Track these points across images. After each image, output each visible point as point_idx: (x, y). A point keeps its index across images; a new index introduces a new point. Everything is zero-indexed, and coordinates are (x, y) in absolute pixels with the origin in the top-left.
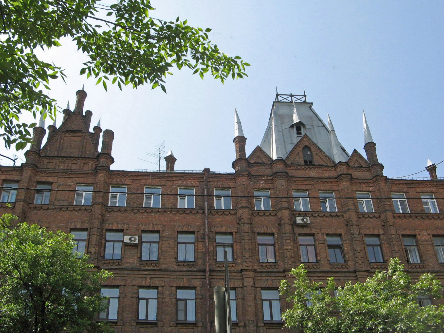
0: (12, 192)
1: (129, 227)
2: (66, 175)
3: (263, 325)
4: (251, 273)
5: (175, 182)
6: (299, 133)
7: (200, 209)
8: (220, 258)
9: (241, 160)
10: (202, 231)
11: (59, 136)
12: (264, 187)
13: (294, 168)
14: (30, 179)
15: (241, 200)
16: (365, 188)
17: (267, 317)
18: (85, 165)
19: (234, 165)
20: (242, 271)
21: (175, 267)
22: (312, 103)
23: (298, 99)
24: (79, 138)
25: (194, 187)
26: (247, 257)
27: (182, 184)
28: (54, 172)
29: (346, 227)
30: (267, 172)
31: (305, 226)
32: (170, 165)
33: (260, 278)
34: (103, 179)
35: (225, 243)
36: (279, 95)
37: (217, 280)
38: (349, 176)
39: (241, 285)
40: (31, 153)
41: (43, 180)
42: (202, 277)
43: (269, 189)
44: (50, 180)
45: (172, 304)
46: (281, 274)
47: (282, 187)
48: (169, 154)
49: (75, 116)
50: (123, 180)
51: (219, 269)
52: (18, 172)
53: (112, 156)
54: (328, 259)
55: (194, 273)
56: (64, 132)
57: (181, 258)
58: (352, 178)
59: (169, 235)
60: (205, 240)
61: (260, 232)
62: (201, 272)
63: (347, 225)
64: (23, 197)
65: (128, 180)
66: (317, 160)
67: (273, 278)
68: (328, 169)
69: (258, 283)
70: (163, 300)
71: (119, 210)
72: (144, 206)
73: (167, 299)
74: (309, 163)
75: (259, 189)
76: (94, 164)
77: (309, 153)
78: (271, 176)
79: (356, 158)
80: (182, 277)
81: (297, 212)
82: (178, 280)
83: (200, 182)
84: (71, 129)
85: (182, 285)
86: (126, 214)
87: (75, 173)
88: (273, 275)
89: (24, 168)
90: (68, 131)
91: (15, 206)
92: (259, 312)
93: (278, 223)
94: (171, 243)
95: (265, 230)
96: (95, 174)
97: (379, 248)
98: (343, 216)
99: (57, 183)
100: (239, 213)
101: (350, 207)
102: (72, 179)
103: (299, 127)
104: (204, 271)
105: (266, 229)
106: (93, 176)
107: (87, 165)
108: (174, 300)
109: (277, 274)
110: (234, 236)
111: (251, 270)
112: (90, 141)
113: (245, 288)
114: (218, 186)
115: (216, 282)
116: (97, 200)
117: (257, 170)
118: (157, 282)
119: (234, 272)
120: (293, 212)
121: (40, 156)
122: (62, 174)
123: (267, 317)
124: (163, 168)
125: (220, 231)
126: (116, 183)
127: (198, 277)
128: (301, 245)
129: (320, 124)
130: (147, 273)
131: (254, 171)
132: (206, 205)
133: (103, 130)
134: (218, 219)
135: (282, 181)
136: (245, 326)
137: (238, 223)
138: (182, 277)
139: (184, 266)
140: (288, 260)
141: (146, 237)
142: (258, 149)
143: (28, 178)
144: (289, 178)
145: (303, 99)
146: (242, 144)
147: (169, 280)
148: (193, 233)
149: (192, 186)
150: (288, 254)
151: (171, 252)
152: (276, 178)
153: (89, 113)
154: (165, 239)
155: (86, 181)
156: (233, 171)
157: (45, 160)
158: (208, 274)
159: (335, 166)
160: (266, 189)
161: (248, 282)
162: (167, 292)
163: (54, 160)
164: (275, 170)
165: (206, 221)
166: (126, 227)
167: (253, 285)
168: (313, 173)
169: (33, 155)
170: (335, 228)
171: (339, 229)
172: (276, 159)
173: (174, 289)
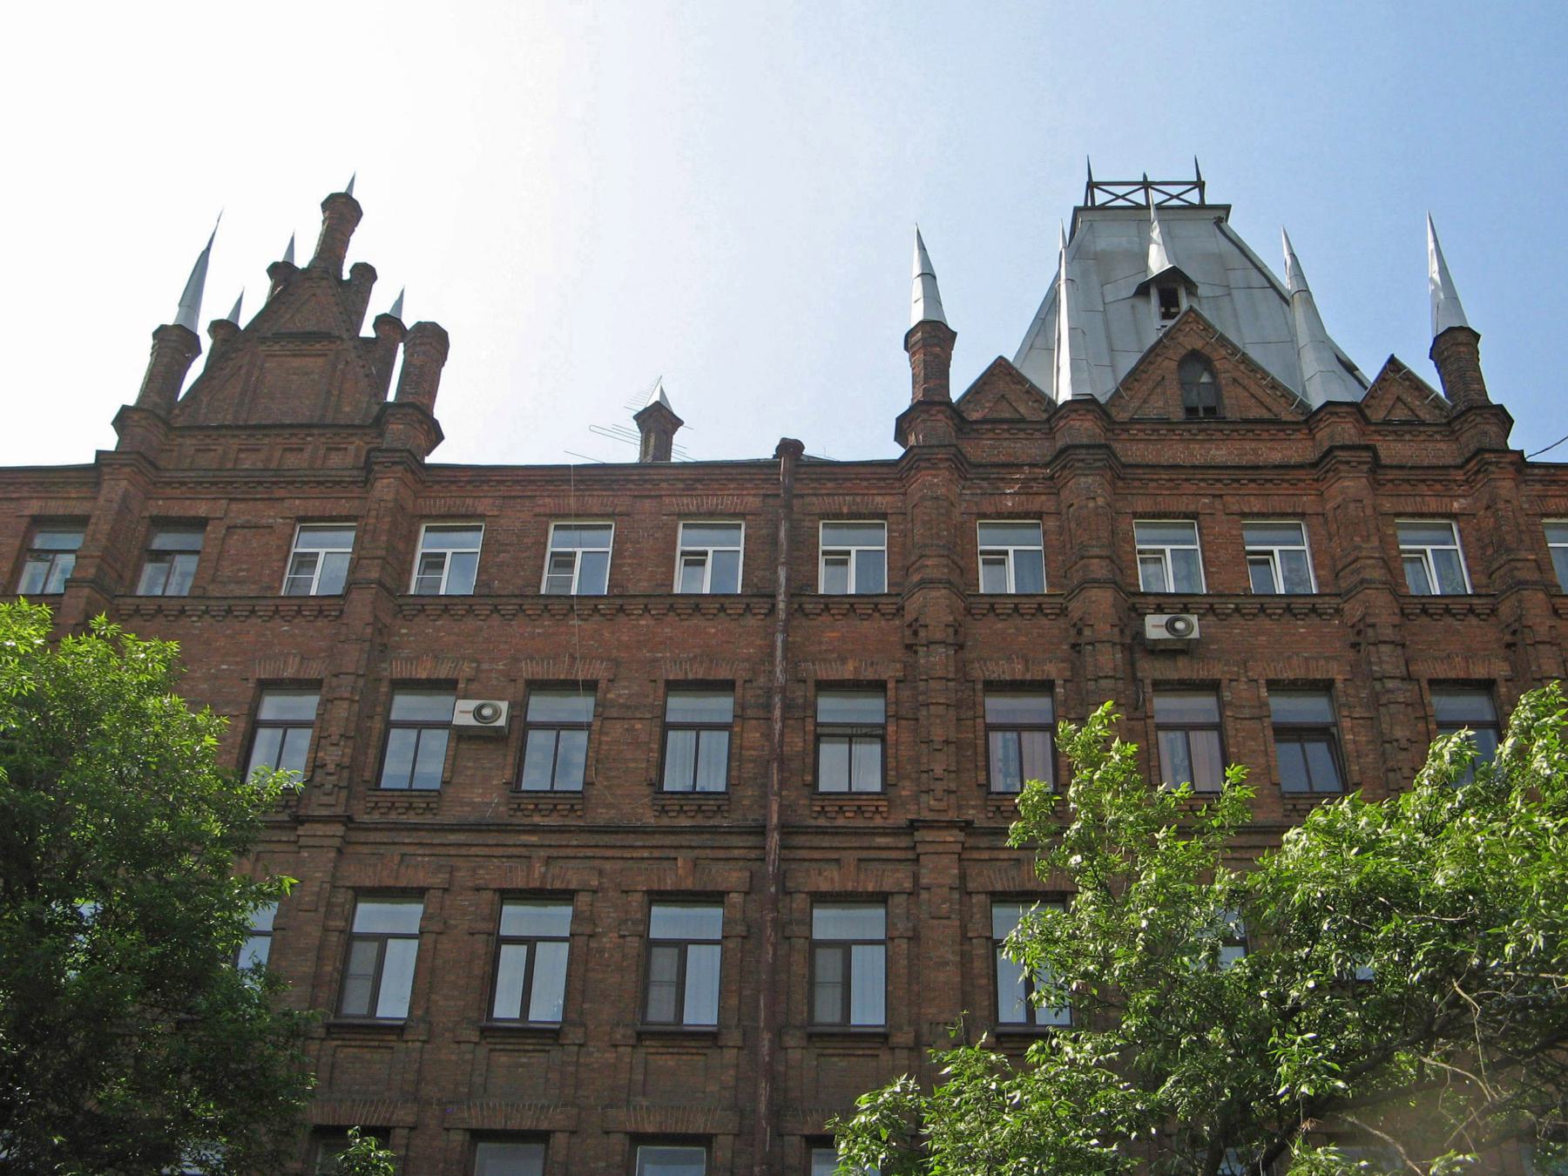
1: (478, 670)
2: (260, 489)
4: (950, 836)
5: (667, 500)
9: (929, 410)
15: (921, 557)
18: (333, 455)
19: (903, 427)
20: (913, 826)
21: (650, 819)
22: (1227, 208)
24: (321, 360)
26: (939, 771)
27: (693, 509)
31: (1183, 652)
32: (652, 441)
33: (986, 855)
34: (390, 497)
37: (814, 865)
38: (1366, 456)
41: (176, 510)
44: (202, 509)
47: (1091, 504)
48: (656, 397)
51: (822, 822)
54: (1275, 779)
57: (675, 780)
59: (630, 696)
61: (994, 676)
62: (750, 833)
63: (1355, 645)
66: (1235, 403)
68: (1281, 435)
69: (980, 874)
74: (1204, 416)
75: (1000, 515)
77: (1205, 379)
78: (1047, 465)
79: (1396, 390)
80: (672, 854)
83: (766, 496)
86: (471, 623)
90: (278, 337)
94: (638, 726)
95: (1018, 671)
98: (1338, 611)
105: (1019, 667)
111: (951, 825)
113: (924, 895)
115: (808, 871)
117: (992, 447)
118: (572, 877)
119: (885, 835)
122: (244, 488)
126: (443, 511)
127: (736, 853)
130: (534, 839)
134: (832, 632)
138: (672, 854)
139: (681, 811)
147: (619, 865)
149: (735, 515)
151: (634, 760)
153: (366, 274)
155: (331, 508)
156: (896, 452)
157: (188, 441)
158: (774, 839)
159: (1311, 419)
160: (1027, 515)
168: (1220, 453)
170: (1306, 659)
171: (1322, 662)
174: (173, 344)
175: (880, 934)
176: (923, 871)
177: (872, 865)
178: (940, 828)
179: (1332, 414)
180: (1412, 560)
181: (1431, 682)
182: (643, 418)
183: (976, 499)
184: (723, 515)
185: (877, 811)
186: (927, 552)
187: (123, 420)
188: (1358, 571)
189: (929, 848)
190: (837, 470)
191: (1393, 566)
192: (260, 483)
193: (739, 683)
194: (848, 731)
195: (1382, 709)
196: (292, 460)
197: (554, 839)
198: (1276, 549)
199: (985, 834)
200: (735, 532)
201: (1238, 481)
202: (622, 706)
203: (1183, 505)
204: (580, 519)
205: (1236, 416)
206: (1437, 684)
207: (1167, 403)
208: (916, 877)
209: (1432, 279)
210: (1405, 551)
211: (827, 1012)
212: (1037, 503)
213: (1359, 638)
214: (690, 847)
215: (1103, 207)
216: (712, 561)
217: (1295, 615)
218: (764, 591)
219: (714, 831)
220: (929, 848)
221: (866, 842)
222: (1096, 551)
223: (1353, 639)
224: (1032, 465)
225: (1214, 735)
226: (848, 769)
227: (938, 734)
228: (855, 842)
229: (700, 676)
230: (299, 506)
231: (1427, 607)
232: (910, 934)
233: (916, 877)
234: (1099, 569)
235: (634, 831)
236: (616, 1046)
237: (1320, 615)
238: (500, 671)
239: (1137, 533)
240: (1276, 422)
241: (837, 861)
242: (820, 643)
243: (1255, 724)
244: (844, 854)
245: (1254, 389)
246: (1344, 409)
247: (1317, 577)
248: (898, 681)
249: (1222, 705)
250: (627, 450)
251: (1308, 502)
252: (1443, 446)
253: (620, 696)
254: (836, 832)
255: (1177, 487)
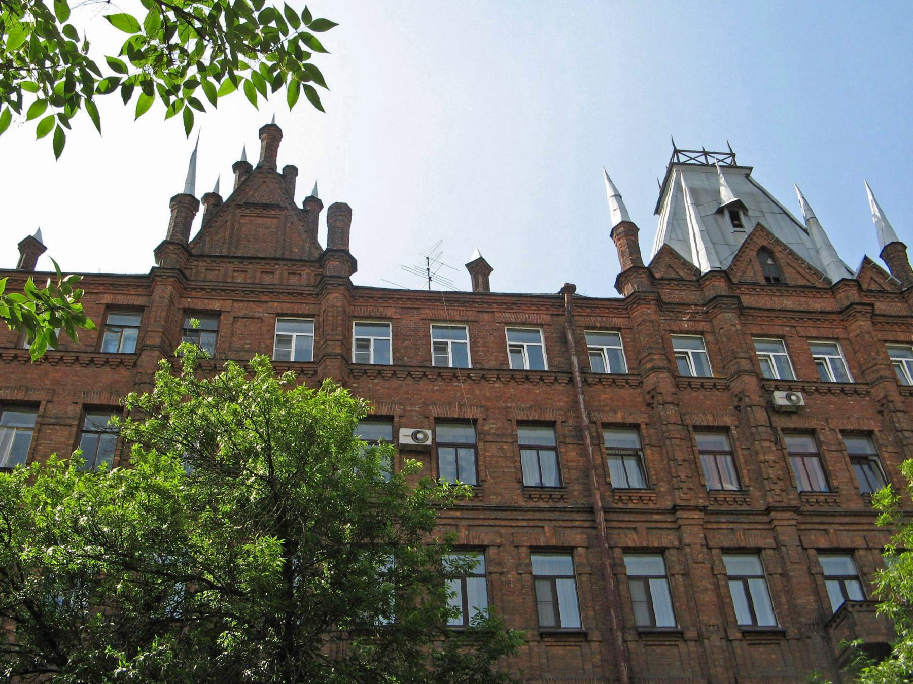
0: (127, 332)
1: (404, 410)
2: (252, 295)
3: (739, 635)
4: (697, 515)
5: (497, 315)
6: (736, 222)
7: (561, 374)
8: (616, 481)
9: (631, 269)
10: (571, 422)
11: (230, 217)
12: (692, 329)
13: (746, 291)
14: (172, 302)
15: (650, 354)
16: (902, 337)
17: (743, 619)
18: (292, 277)
20: (674, 509)
21: (522, 503)
22: (751, 169)
23: (691, 159)
24: (275, 221)
25: (541, 325)
26: (683, 477)
27: (513, 320)
28: (224, 290)
29: (879, 417)
30: (693, 297)
31: (794, 413)
33: (715, 526)
34: (339, 304)
35: (624, 449)
36: (680, 151)
37: (621, 531)
38: (869, 309)
39: (676, 543)
40: (172, 247)
41: (200, 305)
42: (586, 524)
43: (702, 333)
44: (216, 306)
45: (523, 587)
46: (760, 517)
47: (734, 329)
49: (260, 175)
50: (381, 309)
51: (620, 505)
52: (140, 289)
53: (351, 252)
54: (856, 485)
55: (567, 516)
56: (239, 206)
57: (531, 479)
58: (874, 315)
59: (497, 429)
60: (579, 438)
61: (698, 423)
62: (582, 512)
63: (880, 412)
64: (158, 341)
65: (393, 310)
66: (790, 276)
67: (745, 526)
68: (818, 295)
69: (714, 537)
70: (503, 579)
71: (380, 373)
72: (354, 361)
73: (512, 576)
74: (775, 282)
75: (681, 332)
76: (313, 274)
77: (770, 262)
78: (703, 306)
79: (870, 274)
80: (540, 524)
81: (772, 382)
82: (531, 530)
83: (552, 315)
84: (256, 199)
85: (542, 543)
86: (395, 382)
87: (272, 292)
88: (742, 518)
89: (158, 278)
90: (248, 205)
91: (139, 362)
92: (724, 605)
93: (736, 404)
94: (505, 447)
95: (709, 420)
96: (318, 295)
97: (729, 458)
98: (868, 393)
99: (232, 314)
100: (650, 380)
101: (882, 373)
102: (264, 305)
103: (735, 211)
104: (591, 510)
105: (710, 418)
106: (312, 300)
107: (297, 277)
108: (527, 577)
109: (751, 517)
110: (644, 431)
111: (696, 508)
112: (300, 227)
113: (688, 550)
114: (592, 324)
115: (619, 534)
116: (329, 350)
117: (670, 293)
118: (485, 537)
119: (658, 513)
120: (763, 382)
121: (190, 255)
122: (242, 294)
123: (743, 619)
124: (464, 284)
125: (611, 420)
126: (367, 314)
127: (577, 524)
128: (702, 452)
129: (776, 210)
130: (458, 514)
131: (669, 294)
132: (576, 363)
133: (327, 204)
134: (605, 395)
135: (730, 314)
136: (699, 639)
137: (649, 405)
138: (540, 524)
139: (540, 498)
140: (774, 487)
141: (447, 433)
142: (666, 252)
143: (167, 301)
144: (742, 310)
145: (729, 161)
146: (633, 238)
147: (510, 530)
148: (551, 424)
149: (537, 325)
150: (770, 471)
151: (507, 467)
152: (716, 310)
153: (291, 171)
154: (489, 438)
155: (296, 308)
157: (201, 264)
158: (601, 516)
159: (833, 289)
160: (695, 333)
161: (693, 535)
162: (510, 561)
163: (222, 264)
164: (710, 293)
165: (581, 398)
166: (397, 410)
167: (704, 542)
168: (789, 303)
169: (177, 251)
170: (858, 418)
171: (866, 421)
172: (709, 269)
173: (524, 551)
174: (183, 205)
175: (570, 573)
176: (685, 535)
177: (654, 531)
178: (690, 510)
179: (846, 285)
180: (594, 355)
181: (783, 429)
182: (470, 266)
183: (668, 322)
184: (530, 324)
185: (650, 500)
186: (653, 351)
187: (159, 252)
188: (877, 371)
189: (687, 522)
190: (591, 302)
191: (670, 361)
192: (252, 292)
193: (559, 423)
194: (623, 452)
195: (905, 448)
196: (267, 279)
197: (470, 514)
198: (525, 344)
199: (712, 514)
200: (384, 329)
201: (802, 319)
202: (494, 434)
203: (776, 330)
204: (380, 320)
205: (793, 283)
206: (699, 429)
207: (755, 273)
208: (680, 540)
209: (875, 215)
210: (760, 356)
211: (642, 619)
212: (701, 326)
213: (651, 401)
214: (550, 520)
215: (684, 164)
216: (529, 352)
217: (692, 388)
218: (561, 370)
219: (562, 510)
220: (687, 522)
221: (648, 517)
222: (742, 355)
223: (880, 409)
224: (696, 305)
225: (553, 453)
226: (623, 475)
227: (679, 456)
228: (643, 518)
229: (536, 418)
230: (277, 306)
231: (601, 378)
232: (683, 572)
233: (680, 540)
234: (745, 365)
235: (516, 510)
236: (528, 642)
237: (859, 395)
238: (418, 412)
239: (587, 338)
240: (815, 288)
241: (635, 529)
242: (599, 401)
243: (839, 454)
244: (638, 525)
245: (799, 269)
246: (851, 283)
247: (852, 373)
248: (647, 424)
249: (478, 434)
250: (464, 284)
251: (839, 332)
252: (898, 304)
253: (491, 428)
254: (631, 511)
255: (772, 321)
